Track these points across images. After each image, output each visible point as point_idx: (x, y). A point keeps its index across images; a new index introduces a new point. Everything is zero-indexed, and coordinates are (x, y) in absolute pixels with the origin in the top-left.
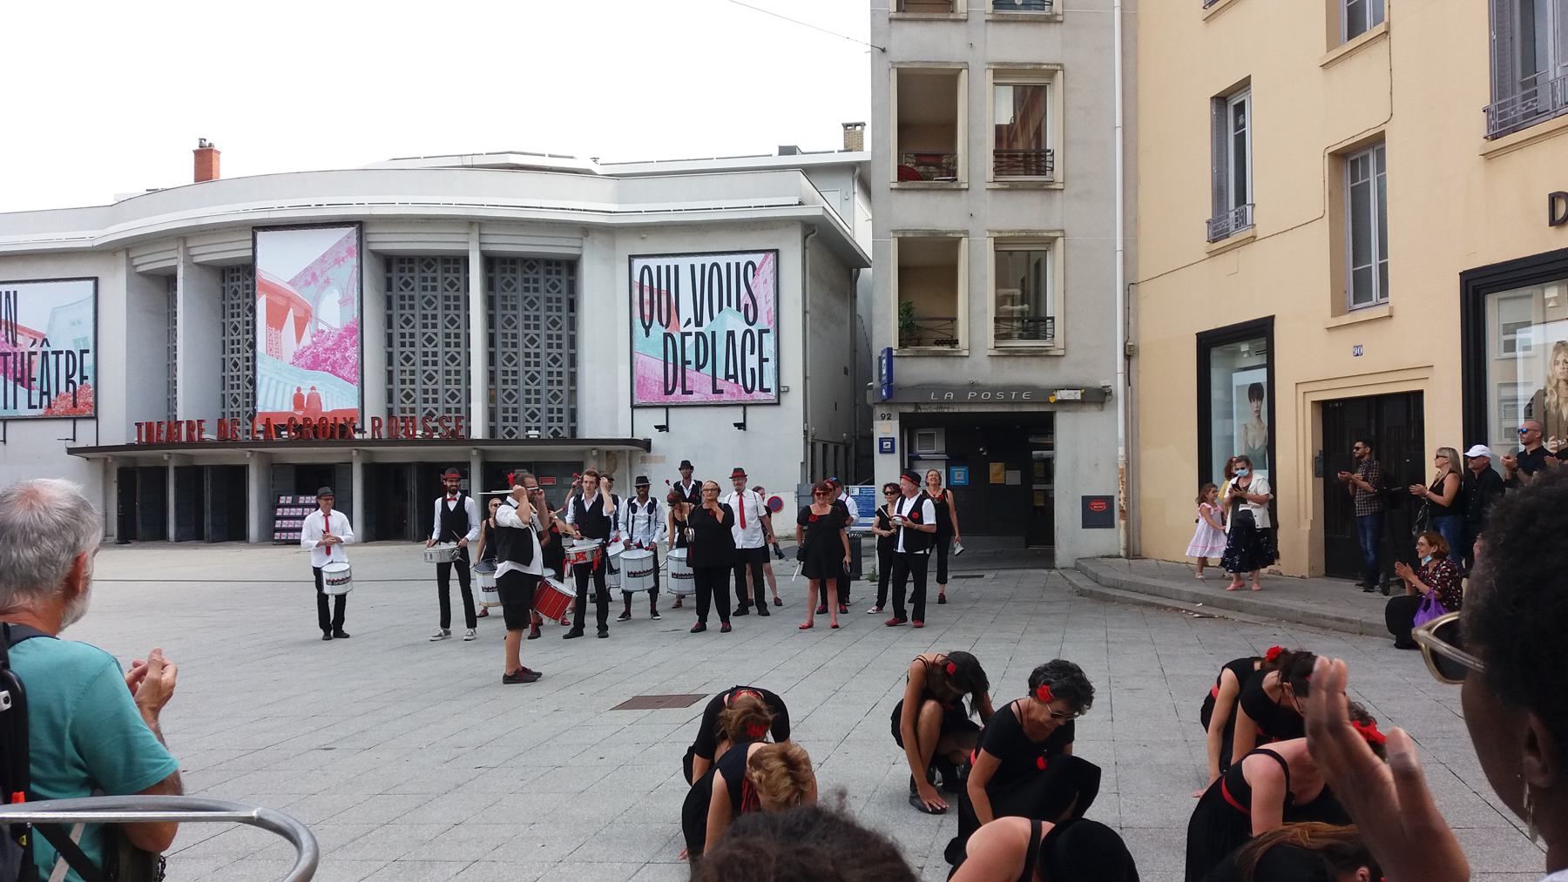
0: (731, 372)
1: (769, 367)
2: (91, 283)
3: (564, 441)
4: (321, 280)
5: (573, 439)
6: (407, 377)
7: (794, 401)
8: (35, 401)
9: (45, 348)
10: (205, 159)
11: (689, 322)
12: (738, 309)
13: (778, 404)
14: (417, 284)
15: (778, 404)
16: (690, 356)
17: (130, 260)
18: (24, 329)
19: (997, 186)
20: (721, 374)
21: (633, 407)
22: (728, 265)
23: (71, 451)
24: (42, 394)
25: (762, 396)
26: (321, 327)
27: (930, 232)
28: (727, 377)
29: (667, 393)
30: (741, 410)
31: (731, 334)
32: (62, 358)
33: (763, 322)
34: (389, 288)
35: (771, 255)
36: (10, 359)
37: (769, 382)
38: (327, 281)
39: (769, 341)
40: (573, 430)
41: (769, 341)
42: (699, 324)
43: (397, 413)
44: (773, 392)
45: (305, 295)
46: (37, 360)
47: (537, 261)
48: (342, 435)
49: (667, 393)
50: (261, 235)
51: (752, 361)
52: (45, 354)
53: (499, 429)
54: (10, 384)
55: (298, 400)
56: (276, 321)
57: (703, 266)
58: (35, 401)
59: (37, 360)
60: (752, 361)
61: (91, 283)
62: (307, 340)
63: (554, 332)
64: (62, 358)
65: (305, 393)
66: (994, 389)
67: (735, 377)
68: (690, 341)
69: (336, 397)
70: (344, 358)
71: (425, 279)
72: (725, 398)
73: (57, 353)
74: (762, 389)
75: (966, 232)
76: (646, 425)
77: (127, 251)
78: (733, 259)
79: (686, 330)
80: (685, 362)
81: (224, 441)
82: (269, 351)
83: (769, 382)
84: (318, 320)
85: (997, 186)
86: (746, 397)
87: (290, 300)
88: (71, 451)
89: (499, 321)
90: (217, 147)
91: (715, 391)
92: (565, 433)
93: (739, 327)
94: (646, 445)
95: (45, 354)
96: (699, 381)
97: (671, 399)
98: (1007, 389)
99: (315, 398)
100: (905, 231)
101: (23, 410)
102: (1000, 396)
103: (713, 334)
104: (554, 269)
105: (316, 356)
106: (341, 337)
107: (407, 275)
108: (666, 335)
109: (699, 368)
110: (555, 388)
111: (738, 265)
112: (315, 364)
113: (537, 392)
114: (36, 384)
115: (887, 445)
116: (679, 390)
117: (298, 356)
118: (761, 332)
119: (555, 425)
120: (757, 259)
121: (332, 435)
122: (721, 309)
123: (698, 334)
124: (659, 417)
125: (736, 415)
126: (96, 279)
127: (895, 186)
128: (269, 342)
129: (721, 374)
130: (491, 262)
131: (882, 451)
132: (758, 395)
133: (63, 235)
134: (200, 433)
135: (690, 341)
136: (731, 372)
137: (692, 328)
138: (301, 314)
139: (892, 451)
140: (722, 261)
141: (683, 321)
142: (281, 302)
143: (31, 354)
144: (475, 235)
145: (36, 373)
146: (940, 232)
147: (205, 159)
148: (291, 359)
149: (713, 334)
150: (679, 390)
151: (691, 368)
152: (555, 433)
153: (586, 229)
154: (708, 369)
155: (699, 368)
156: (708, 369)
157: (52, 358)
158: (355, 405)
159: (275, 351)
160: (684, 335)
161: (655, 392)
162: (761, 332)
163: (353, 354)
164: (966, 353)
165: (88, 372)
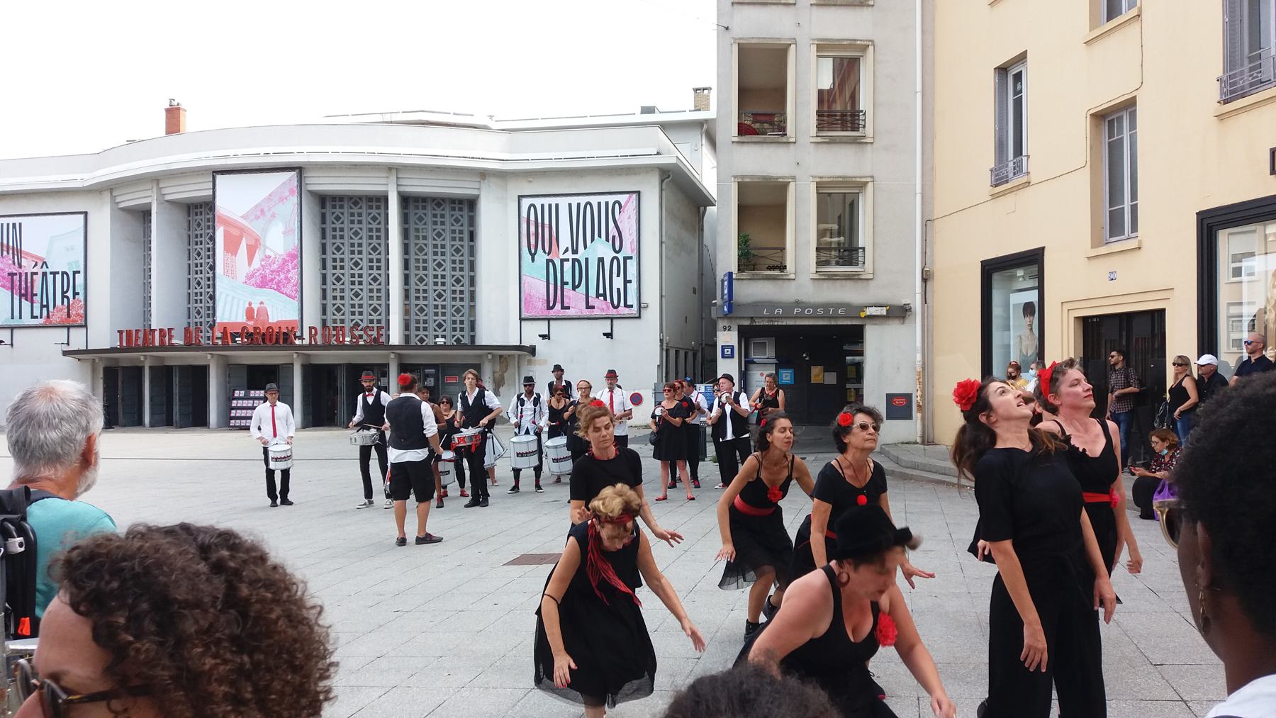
0: (601, 291)
1: (632, 288)
2: (82, 216)
3: (465, 347)
4: (268, 214)
5: (473, 345)
6: (338, 294)
7: (652, 316)
8: (37, 313)
9: (45, 269)
10: (173, 117)
11: (567, 250)
12: (607, 240)
13: (639, 317)
14: (346, 218)
15: (639, 317)
16: (568, 278)
17: (113, 198)
18: (27, 254)
19: (819, 140)
20: (592, 292)
21: (521, 319)
22: (599, 204)
23: (66, 353)
24: (42, 306)
25: (626, 311)
26: (268, 253)
27: (764, 177)
28: (598, 295)
29: (549, 308)
30: (9, 331)
31: (601, 260)
32: (59, 277)
33: (627, 250)
34: (324, 222)
35: (634, 196)
36: (16, 278)
37: (632, 299)
38: (273, 216)
39: (632, 265)
40: (473, 338)
41: (632, 265)
42: (575, 252)
43: (330, 324)
44: (635, 308)
45: (255, 227)
46: (38, 279)
47: (443, 200)
48: (285, 340)
49: (549, 308)
50: (219, 178)
51: (618, 283)
52: (44, 274)
53: (413, 337)
54: (16, 298)
55: (250, 312)
56: (232, 248)
57: (579, 205)
58: (37, 313)
59: (38, 279)
60: (618, 283)
61: (82, 216)
62: (257, 263)
63: (457, 258)
64: (59, 277)
65: (255, 307)
66: (815, 306)
67: (604, 295)
68: (568, 265)
69: (280, 311)
70: (287, 278)
71: (352, 215)
72: (596, 312)
73: (54, 274)
74: (626, 306)
75: (794, 178)
76: (531, 333)
77: (111, 190)
78: (603, 199)
79: (565, 257)
80: (564, 283)
81: (189, 346)
82: (226, 272)
83: (632, 299)
84: (266, 247)
85: (819, 140)
86: (613, 312)
87: (243, 230)
88: (66, 353)
89: (412, 249)
90: (182, 106)
91: (588, 307)
92: (466, 341)
93: (608, 254)
94: (532, 350)
95: (44, 274)
96: (575, 299)
97: (552, 313)
98: (826, 306)
99: (263, 311)
100: (743, 177)
101: (27, 320)
102: (820, 312)
103: (587, 260)
104: (457, 206)
105: (263, 277)
106: (285, 262)
107: (338, 211)
108: (548, 261)
109: (575, 287)
110: (458, 303)
111: (607, 204)
112: (263, 283)
113: (444, 307)
114: (37, 299)
115: (728, 352)
116: (558, 306)
117: (250, 277)
118: (626, 259)
119: (458, 334)
120: (623, 199)
121: (277, 341)
122: (593, 240)
123: (574, 260)
124: (542, 327)
125: (605, 326)
126: (86, 213)
127: (736, 139)
128: (226, 265)
129: (592, 292)
130: (406, 200)
131: (723, 356)
132: (623, 310)
133: (59, 177)
134: (170, 339)
135: (568, 265)
136: (601, 291)
137: (569, 255)
138: (253, 243)
139: (732, 356)
140: (594, 200)
141: (562, 249)
142: (236, 232)
143: (33, 274)
144: (393, 178)
145: (37, 290)
146: (772, 177)
147: (173, 117)
148: (244, 279)
149: (587, 260)
150: (558, 306)
151: (568, 288)
152: (458, 340)
153: (483, 174)
154: (582, 288)
155: (575, 287)
156: (582, 288)
157: (50, 278)
158: (296, 317)
159: (230, 272)
160: (562, 261)
161: (539, 308)
162: (626, 259)
163: (294, 275)
164: (870, 276)
165: (80, 289)
